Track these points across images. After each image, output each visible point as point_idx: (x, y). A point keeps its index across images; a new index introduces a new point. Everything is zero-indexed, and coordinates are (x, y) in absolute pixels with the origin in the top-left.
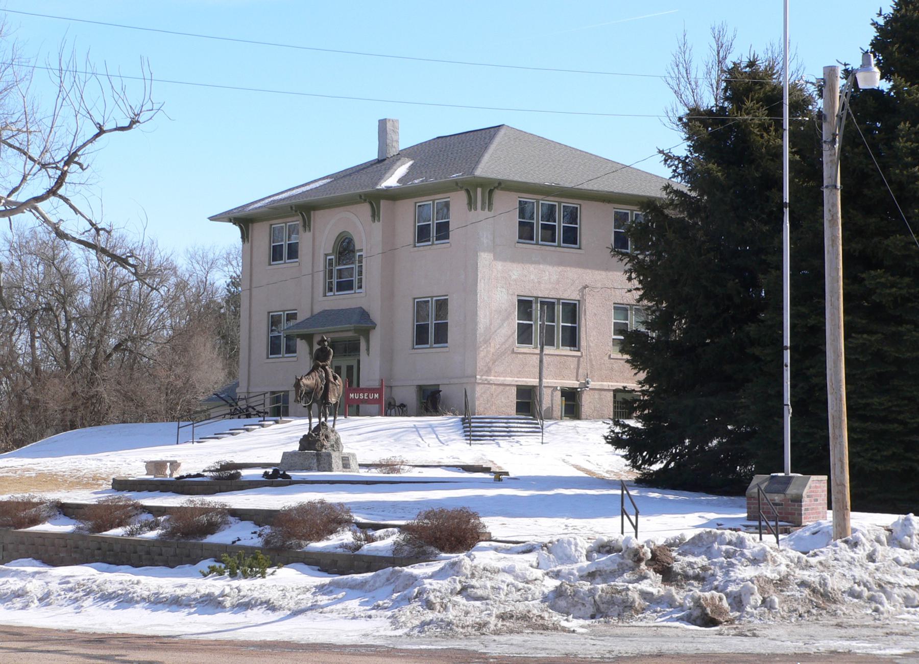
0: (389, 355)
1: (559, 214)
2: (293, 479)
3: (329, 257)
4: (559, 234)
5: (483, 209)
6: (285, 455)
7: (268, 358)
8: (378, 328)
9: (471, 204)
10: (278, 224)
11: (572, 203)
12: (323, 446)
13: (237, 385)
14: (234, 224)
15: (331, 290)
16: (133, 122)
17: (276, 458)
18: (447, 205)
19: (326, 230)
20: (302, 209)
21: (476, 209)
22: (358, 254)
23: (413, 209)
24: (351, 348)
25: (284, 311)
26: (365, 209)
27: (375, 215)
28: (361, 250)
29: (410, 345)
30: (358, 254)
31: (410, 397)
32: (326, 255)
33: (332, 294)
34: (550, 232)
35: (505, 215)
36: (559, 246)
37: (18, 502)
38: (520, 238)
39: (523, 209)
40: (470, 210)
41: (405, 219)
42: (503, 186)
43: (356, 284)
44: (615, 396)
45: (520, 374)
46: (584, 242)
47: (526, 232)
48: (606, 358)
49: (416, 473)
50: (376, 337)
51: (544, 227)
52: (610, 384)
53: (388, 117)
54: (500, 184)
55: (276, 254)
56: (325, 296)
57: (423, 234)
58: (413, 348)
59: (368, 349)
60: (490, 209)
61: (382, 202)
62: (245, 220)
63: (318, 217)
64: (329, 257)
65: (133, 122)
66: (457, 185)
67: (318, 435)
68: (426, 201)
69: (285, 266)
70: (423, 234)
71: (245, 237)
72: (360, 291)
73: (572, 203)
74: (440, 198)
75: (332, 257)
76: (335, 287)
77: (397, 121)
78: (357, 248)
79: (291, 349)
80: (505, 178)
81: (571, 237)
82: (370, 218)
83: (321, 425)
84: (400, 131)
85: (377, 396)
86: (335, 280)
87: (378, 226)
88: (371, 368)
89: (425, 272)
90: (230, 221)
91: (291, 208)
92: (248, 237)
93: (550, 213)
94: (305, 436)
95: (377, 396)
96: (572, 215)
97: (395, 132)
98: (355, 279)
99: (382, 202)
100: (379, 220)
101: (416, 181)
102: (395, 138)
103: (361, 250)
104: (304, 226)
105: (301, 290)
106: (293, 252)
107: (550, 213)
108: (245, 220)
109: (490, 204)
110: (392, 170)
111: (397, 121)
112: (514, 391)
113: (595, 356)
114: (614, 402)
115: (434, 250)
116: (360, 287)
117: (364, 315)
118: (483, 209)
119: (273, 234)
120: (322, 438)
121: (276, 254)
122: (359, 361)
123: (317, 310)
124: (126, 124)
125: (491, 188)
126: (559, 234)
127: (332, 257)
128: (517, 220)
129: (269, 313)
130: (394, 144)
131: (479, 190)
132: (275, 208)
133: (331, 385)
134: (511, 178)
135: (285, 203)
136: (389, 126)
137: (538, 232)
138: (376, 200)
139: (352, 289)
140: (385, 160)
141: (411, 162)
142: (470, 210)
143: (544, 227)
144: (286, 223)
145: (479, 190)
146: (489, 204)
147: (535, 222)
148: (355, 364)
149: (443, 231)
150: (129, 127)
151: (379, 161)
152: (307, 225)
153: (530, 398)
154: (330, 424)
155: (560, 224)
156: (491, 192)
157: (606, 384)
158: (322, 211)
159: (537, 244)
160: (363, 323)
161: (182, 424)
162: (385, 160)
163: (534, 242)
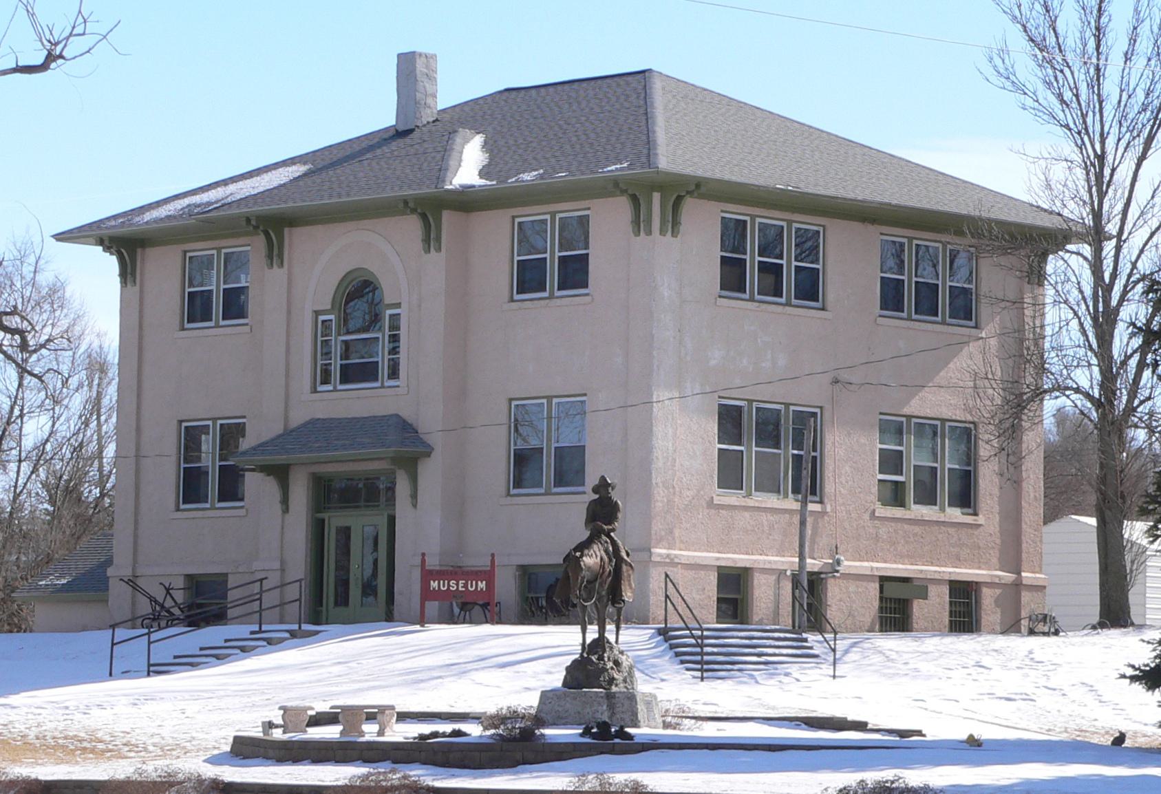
0: (458, 506)
1: (789, 246)
2: (636, 740)
3: (322, 318)
4: (789, 281)
5: (663, 232)
6: (544, 695)
7: (178, 509)
8: (437, 456)
9: (639, 223)
10: (201, 249)
11: (809, 223)
12: (612, 680)
13: (109, 562)
14: (107, 249)
15: (325, 381)
16: (51, 58)
17: (529, 701)
18: (584, 222)
19: (318, 266)
20: (268, 223)
21: (649, 233)
22: (389, 312)
23: (509, 226)
24: (369, 493)
25: (214, 420)
26: (411, 226)
27: (431, 238)
28: (398, 305)
29: (503, 490)
30: (389, 312)
31: (507, 588)
32: (317, 313)
33: (330, 387)
34: (770, 279)
35: (698, 243)
36: (788, 304)
37: (155, 783)
38: (722, 289)
39: (734, 234)
40: (637, 233)
41: (493, 247)
42: (703, 190)
43: (384, 370)
44: (881, 587)
45: (724, 546)
46: (831, 297)
47: (733, 277)
48: (867, 516)
49: (710, 731)
50: (431, 473)
51: (763, 267)
52: (875, 565)
53: (418, 49)
54: (698, 186)
55: (197, 308)
56: (315, 391)
57: (529, 279)
58: (508, 494)
59: (414, 496)
60: (674, 234)
61: (446, 216)
62: (127, 242)
63: (298, 241)
64: (322, 318)
65: (51, 58)
66: (615, 187)
67: (601, 658)
68: (531, 214)
69: (218, 336)
70: (529, 279)
71: (127, 273)
72: (392, 383)
73: (809, 223)
74: (570, 210)
75: (332, 317)
76: (336, 373)
77: (434, 57)
78: (387, 301)
79: (231, 489)
80: (708, 175)
81: (809, 289)
82: (418, 244)
83: (599, 645)
84: (440, 76)
85: (482, 585)
86: (336, 364)
87: (436, 260)
88: (421, 528)
89: (539, 349)
90: (100, 242)
91: (248, 220)
92: (133, 274)
93: (770, 245)
94: (575, 662)
95: (482, 585)
96: (809, 246)
97: (431, 78)
98: (382, 359)
99: (446, 216)
100: (439, 249)
101: (527, 177)
102: (430, 90)
103: (398, 305)
104: (270, 256)
105: (266, 375)
106: (235, 305)
107: (770, 245)
108: (127, 242)
109: (676, 223)
110: (455, 154)
111: (434, 57)
112: (713, 578)
113: (849, 512)
114: (881, 599)
115: (554, 310)
116: (394, 373)
117: (406, 428)
118: (663, 232)
119: (194, 268)
120: (610, 665)
121: (197, 308)
122: (392, 521)
123: (298, 417)
124: (39, 59)
125: (678, 193)
126: (789, 281)
127: (332, 317)
128: (717, 253)
129: (181, 422)
130: (430, 101)
131: (656, 196)
132: (209, 221)
133: (624, 568)
134: (718, 175)
135: (235, 211)
136: (420, 66)
137: (752, 276)
138: (435, 210)
139: (376, 379)
140: (411, 131)
141: (478, 140)
142: (637, 233)
143: (763, 267)
144: (219, 249)
145: (656, 196)
146: (673, 223)
147: (748, 257)
148: (383, 522)
149: (575, 273)
150: (43, 67)
151: (399, 134)
152: (274, 254)
153: (738, 591)
154: (611, 637)
155: (789, 263)
156: (679, 199)
157: (864, 566)
158: (320, 227)
159: (752, 299)
160: (407, 446)
161: (121, 633)
162: (411, 131)
163: (747, 296)
